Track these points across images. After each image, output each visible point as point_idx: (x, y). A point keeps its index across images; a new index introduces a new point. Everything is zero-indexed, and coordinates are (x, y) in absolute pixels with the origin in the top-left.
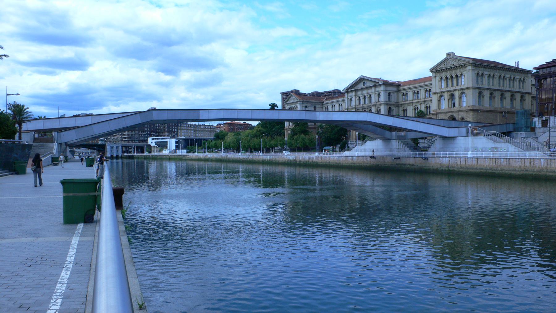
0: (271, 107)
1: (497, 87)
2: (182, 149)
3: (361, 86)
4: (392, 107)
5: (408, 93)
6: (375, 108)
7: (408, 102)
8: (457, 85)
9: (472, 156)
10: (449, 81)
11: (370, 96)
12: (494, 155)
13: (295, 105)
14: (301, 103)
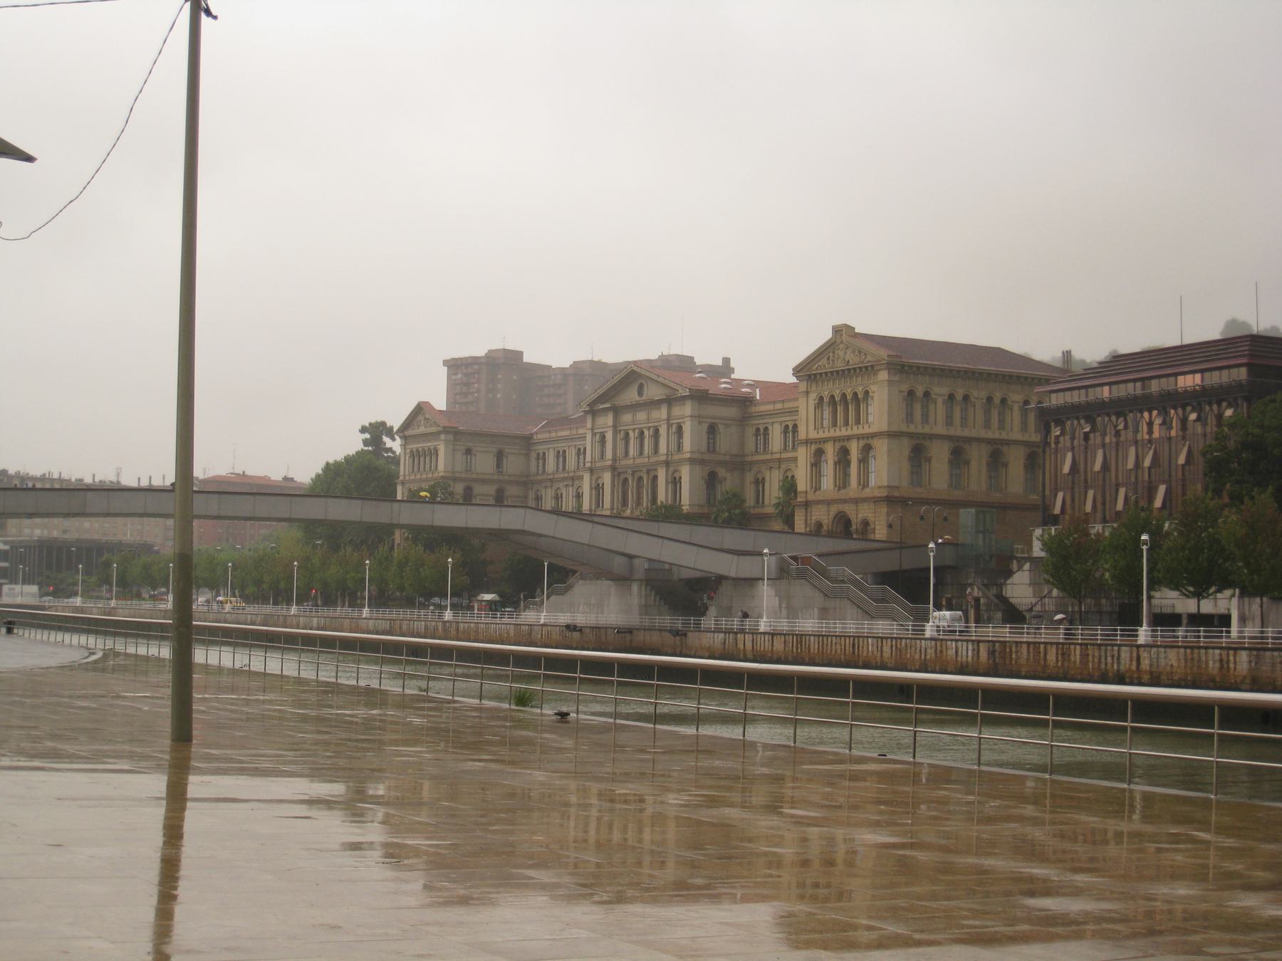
0: (367, 436)
1: (978, 432)
2: (24, 583)
3: (631, 396)
4: (721, 472)
5: (770, 428)
6: (667, 472)
7: (769, 457)
8: (858, 422)
9: (768, 629)
10: (840, 409)
11: (657, 431)
12: (1186, 637)
13: (430, 444)
14: (451, 437)
